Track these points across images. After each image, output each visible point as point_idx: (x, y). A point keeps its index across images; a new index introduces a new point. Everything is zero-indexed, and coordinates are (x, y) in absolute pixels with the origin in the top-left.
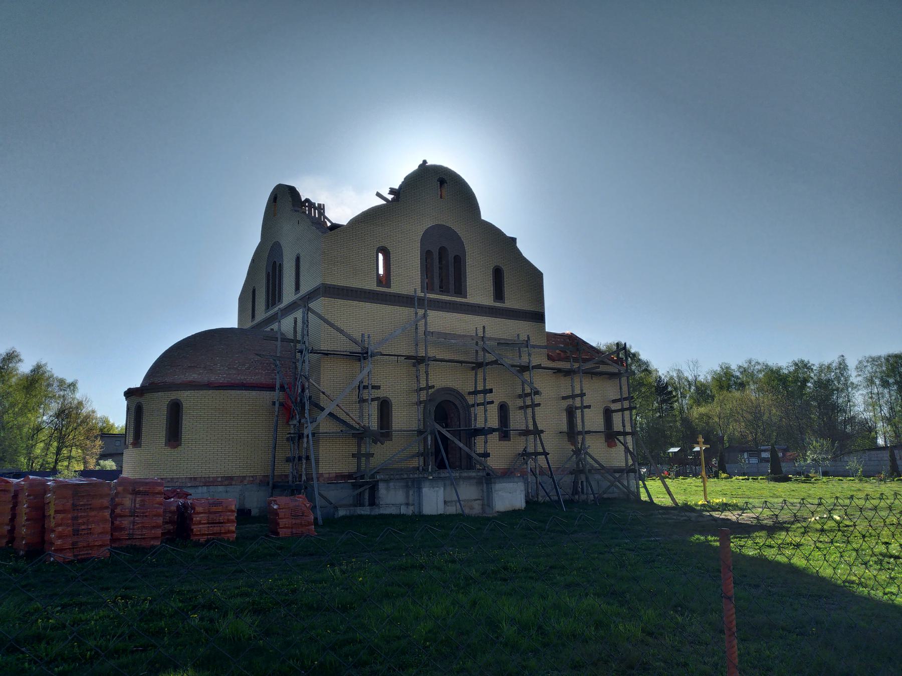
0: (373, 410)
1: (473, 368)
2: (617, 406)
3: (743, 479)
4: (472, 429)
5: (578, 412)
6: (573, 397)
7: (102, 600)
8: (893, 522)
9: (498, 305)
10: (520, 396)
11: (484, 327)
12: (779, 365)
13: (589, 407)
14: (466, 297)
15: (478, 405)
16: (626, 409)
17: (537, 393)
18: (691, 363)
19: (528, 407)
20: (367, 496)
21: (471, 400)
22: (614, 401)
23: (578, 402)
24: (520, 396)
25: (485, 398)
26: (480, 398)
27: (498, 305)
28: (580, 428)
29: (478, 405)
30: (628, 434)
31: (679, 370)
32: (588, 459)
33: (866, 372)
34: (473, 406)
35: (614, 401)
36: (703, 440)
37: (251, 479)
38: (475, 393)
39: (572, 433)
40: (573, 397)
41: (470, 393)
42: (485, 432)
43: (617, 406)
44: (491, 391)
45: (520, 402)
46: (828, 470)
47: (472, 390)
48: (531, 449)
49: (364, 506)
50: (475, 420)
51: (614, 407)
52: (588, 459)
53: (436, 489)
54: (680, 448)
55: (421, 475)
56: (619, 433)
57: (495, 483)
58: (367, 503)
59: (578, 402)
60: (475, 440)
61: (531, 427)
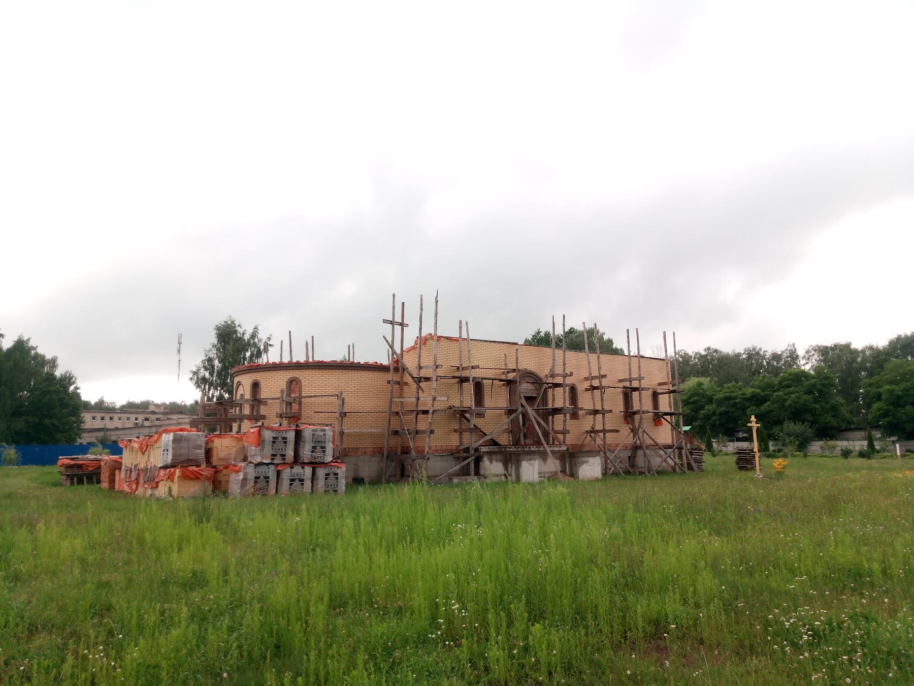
0: (469, 388)
4: (548, 409)
5: (635, 395)
7: (238, 567)
8: (311, 583)
11: (403, 304)
12: (737, 352)
18: (655, 348)
20: (472, 466)
22: (660, 384)
28: (636, 408)
33: (814, 361)
36: (755, 420)
37: (363, 450)
39: (629, 415)
45: (587, 385)
46: (352, 477)
48: (599, 427)
49: (469, 475)
50: (554, 400)
53: (533, 462)
54: (690, 427)
55: (515, 449)
57: (578, 457)
58: (473, 473)
60: (553, 418)
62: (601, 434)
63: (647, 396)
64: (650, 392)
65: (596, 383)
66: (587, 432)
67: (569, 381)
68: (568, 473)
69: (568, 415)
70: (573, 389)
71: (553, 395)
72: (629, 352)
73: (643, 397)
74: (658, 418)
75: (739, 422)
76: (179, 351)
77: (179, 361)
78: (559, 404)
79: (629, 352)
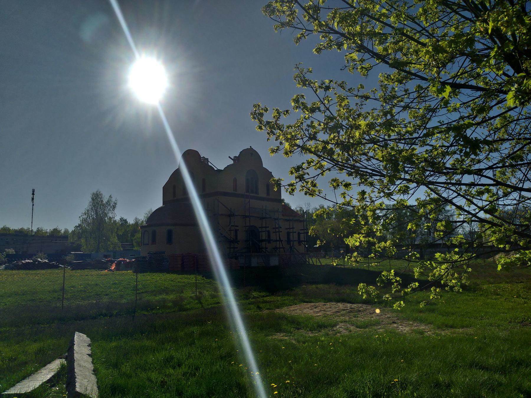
1: (244, 218)
2: (302, 232)
3: (119, 275)
5: (291, 234)
6: (290, 229)
9: (268, 197)
10: (274, 228)
13: (281, 232)
14: (237, 191)
15: (263, 231)
16: (264, 227)
17: (281, 228)
19: (277, 232)
21: (260, 230)
22: (301, 230)
23: (291, 230)
24: (274, 228)
25: (266, 229)
26: (264, 229)
27: (268, 197)
29: (263, 231)
30: (305, 241)
31: (301, 207)
32: (295, 250)
34: (261, 232)
35: (301, 230)
38: (262, 227)
39: (289, 241)
40: (290, 229)
41: (259, 228)
42: (263, 241)
43: (302, 232)
44: (268, 227)
47: (261, 226)
48: (278, 246)
50: (262, 236)
51: (301, 232)
52: (295, 250)
56: (303, 241)
59: (291, 230)
61: (278, 239)
62: (292, 229)
63: (296, 235)
64: (297, 233)
65: (277, 230)
66: (273, 248)
67: (267, 229)
68: (55, 366)
69: (267, 242)
70: (269, 232)
71: (262, 235)
72: (280, 243)
73: (294, 235)
74: (300, 242)
75: (355, 235)
76: (33, 199)
77: (33, 205)
78: (264, 238)
79: (280, 243)
